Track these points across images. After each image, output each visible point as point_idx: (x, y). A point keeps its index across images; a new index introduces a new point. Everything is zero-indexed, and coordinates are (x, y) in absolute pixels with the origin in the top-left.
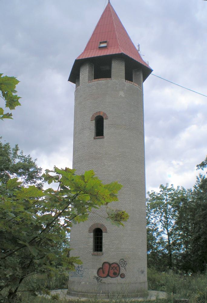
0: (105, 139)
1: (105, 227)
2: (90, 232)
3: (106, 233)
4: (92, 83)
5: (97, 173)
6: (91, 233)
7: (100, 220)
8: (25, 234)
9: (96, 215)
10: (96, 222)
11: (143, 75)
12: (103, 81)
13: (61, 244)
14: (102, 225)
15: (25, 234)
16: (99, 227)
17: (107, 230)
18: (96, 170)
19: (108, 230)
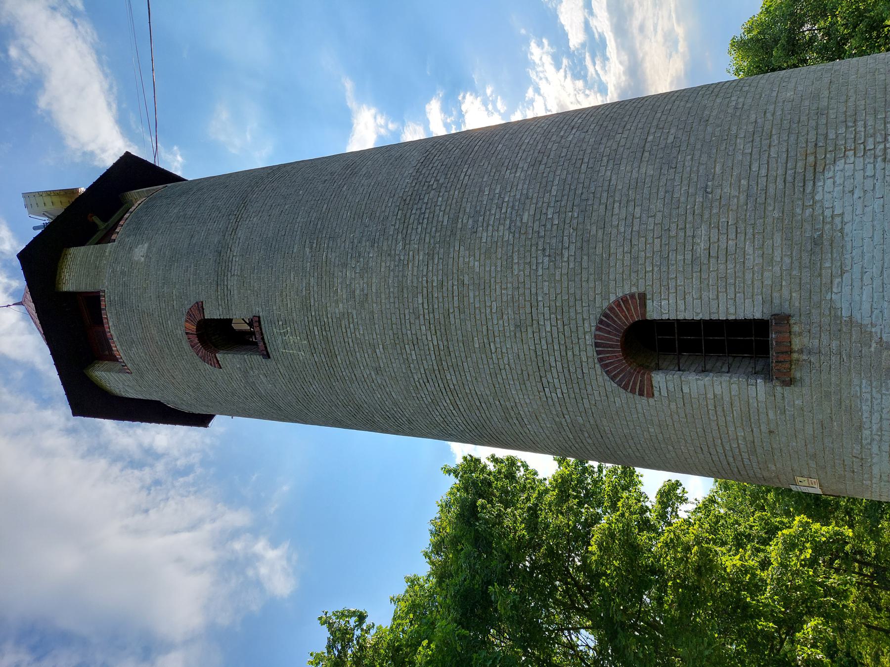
0: (261, 314)
1: (606, 315)
2: (646, 391)
3: (649, 303)
4: (125, 361)
5: (381, 346)
6: (655, 384)
7: (581, 335)
8: (764, 535)
9: (557, 353)
10: (590, 354)
11: (595, 38)
12: (111, 324)
13: (573, 560)
14: (605, 321)
15: (764, 535)
16: (616, 340)
17: (632, 296)
18: (369, 351)
19: (628, 289)
